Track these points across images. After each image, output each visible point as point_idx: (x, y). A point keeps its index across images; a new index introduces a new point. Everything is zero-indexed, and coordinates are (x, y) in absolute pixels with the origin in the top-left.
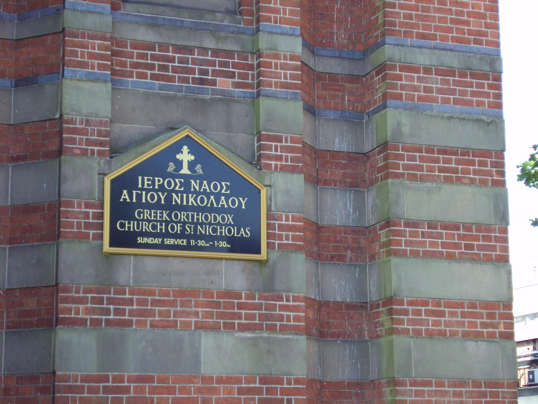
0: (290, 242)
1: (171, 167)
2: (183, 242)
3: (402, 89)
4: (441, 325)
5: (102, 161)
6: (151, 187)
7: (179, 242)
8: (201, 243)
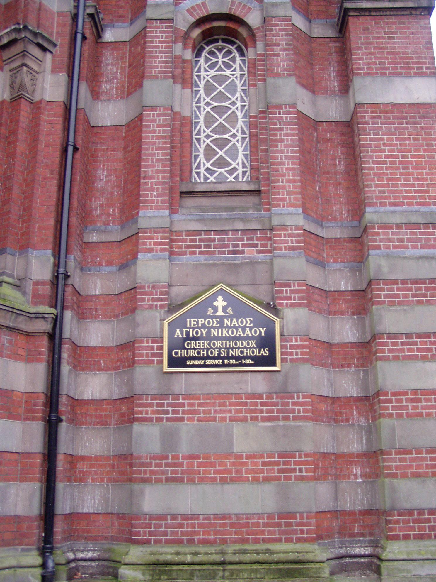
0: (299, 357)
1: (210, 311)
2: (219, 362)
3: (380, 242)
4: (418, 409)
5: (163, 311)
6: (196, 326)
7: (216, 362)
8: (233, 362)
